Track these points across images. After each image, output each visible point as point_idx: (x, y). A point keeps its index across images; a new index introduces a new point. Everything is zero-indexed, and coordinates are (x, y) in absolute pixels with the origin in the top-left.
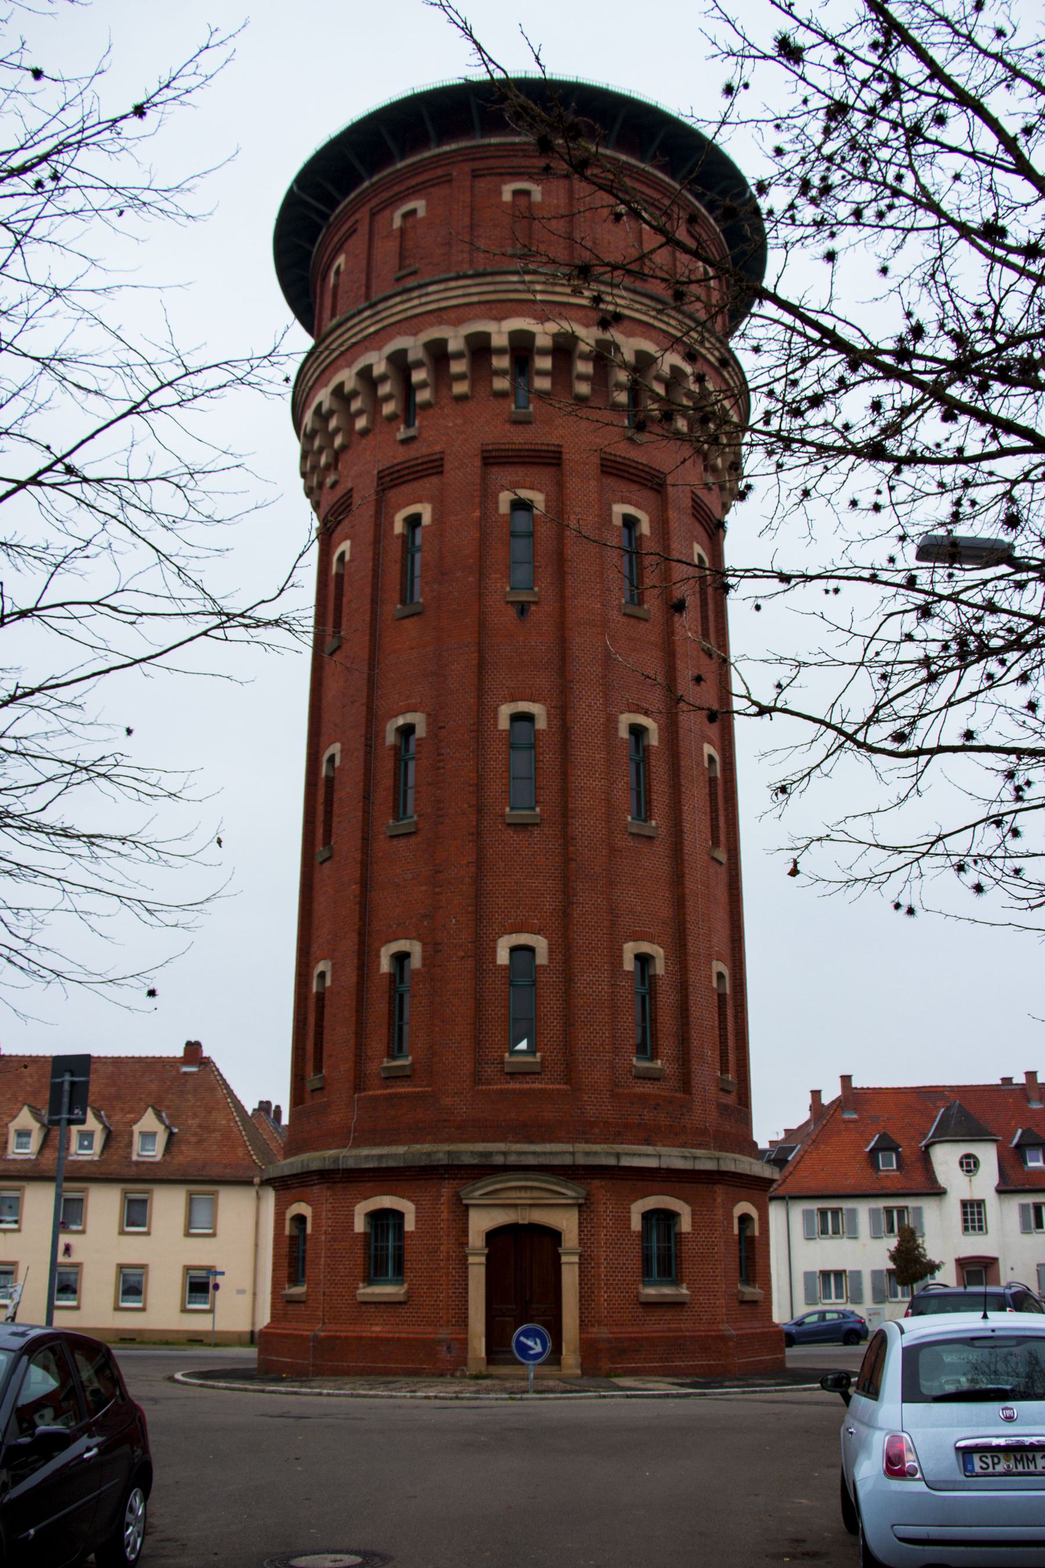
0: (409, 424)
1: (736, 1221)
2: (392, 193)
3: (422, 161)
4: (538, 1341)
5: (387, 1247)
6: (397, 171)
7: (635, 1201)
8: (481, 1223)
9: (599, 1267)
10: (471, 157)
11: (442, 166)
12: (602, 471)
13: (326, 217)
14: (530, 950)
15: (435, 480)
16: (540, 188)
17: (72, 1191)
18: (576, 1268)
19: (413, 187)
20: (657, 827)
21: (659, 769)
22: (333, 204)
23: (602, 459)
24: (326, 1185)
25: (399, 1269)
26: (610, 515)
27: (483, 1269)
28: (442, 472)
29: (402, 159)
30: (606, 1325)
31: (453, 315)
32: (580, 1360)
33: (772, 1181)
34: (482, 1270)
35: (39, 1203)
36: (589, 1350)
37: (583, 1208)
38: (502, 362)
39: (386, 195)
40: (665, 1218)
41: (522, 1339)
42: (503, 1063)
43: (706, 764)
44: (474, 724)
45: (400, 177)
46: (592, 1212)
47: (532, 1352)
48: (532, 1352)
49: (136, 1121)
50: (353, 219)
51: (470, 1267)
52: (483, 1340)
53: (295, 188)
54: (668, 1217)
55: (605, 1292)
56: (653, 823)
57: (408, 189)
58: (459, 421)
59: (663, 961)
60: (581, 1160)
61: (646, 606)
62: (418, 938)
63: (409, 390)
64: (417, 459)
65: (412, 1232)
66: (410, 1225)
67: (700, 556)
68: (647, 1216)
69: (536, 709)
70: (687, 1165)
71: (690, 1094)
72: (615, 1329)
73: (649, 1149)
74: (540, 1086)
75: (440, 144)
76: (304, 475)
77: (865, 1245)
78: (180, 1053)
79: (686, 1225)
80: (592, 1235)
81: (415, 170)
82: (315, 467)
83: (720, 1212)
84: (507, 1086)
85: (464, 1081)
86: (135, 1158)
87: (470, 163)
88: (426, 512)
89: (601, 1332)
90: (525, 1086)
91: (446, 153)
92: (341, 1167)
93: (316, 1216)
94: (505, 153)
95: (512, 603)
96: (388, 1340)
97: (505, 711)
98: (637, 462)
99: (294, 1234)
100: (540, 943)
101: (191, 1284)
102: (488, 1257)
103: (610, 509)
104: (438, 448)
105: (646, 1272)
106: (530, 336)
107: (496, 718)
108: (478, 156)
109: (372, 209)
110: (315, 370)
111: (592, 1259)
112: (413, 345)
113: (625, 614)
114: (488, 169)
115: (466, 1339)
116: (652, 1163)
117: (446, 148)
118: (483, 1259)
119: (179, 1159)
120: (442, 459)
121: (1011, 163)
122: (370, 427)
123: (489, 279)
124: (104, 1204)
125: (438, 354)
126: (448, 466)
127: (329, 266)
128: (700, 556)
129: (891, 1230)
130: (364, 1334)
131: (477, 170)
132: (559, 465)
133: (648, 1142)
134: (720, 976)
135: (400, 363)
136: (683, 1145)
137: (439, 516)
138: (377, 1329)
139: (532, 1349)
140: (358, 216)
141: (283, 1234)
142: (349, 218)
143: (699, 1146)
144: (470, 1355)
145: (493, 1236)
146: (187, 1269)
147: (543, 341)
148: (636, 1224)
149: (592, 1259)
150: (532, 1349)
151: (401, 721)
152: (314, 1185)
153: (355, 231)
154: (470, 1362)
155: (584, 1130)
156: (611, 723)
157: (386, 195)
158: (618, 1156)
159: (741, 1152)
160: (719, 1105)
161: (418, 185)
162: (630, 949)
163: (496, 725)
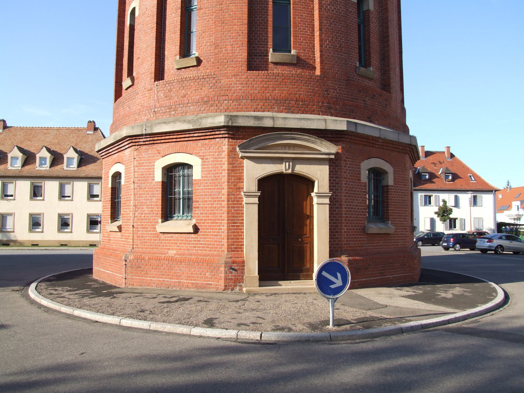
4: (339, 275)
7: (363, 160)
9: (341, 208)
17: (37, 182)
18: (327, 207)
27: (256, 208)
34: (255, 209)
35: (23, 187)
37: (334, 163)
40: (377, 174)
41: (324, 273)
46: (337, 166)
47: (333, 286)
48: (333, 286)
52: (257, 262)
55: (345, 226)
71: (390, 93)
78: (86, 126)
93: (127, 170)
101: (90, 221)
102: (260, 198)
118: (256, 200)
121: (226, 134)
124: (51, 188)
139: (334, 283)
141: (107, 187)
144: (246, 275)
145: (264, 182)
146: (89, 216)
150: (334, 283)
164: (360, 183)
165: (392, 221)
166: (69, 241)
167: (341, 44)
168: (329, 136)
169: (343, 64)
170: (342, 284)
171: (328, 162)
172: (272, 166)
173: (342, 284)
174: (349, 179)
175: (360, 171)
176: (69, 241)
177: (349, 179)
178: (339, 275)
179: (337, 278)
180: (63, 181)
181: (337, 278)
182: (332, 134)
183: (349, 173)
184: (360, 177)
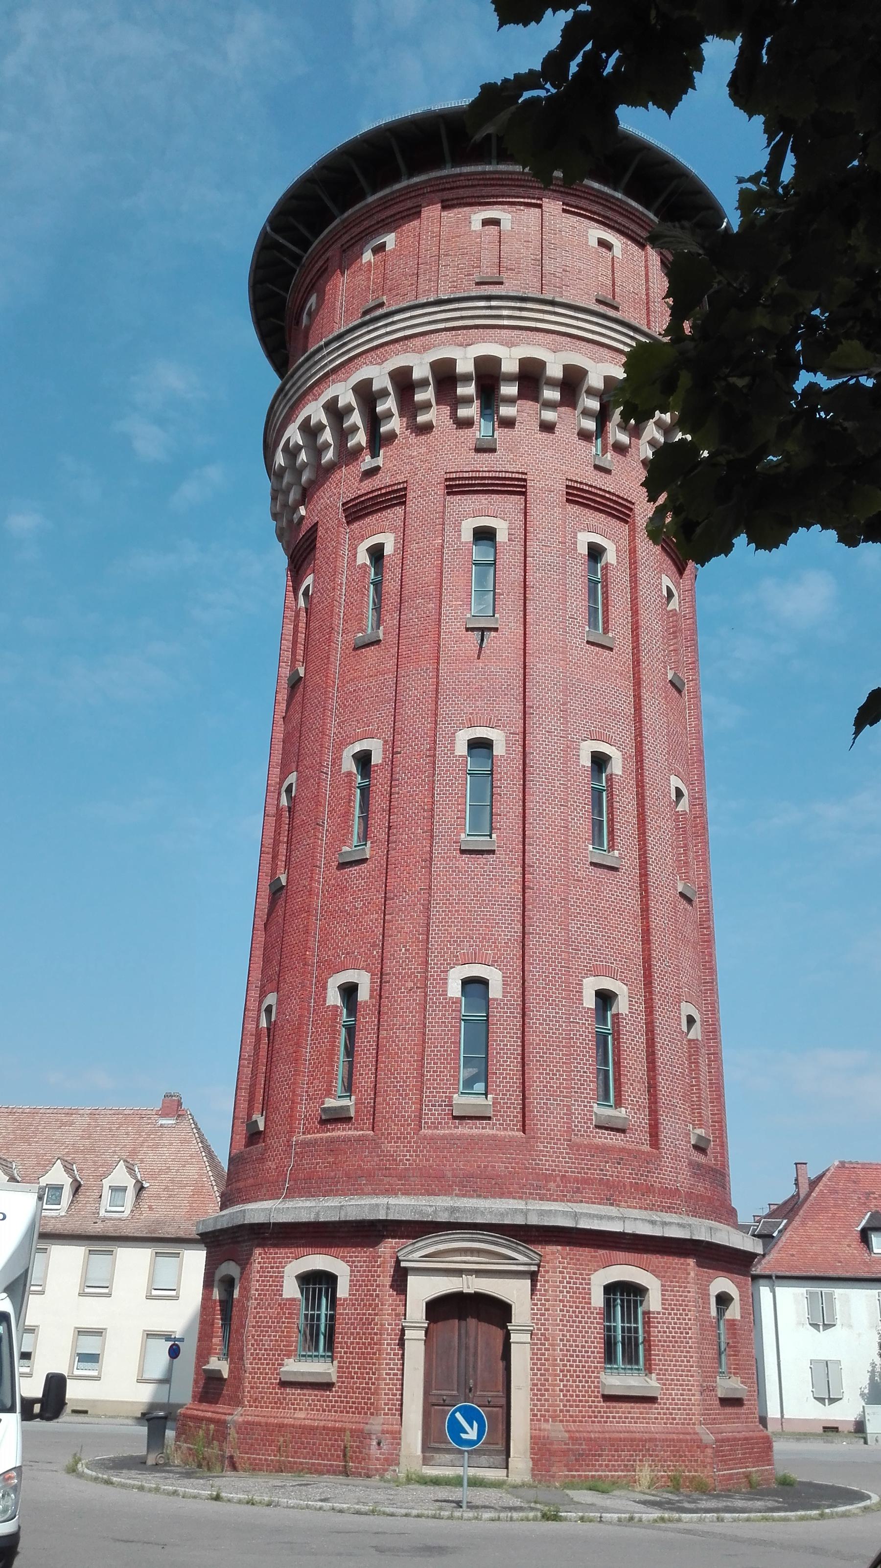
0: (374, 455)
1: (713, 1301)
2: (362, 228)
3: (393, 193)
4: (475, 1425)
5: (319, 1316)
6: (367, 205)
8: (423, 1290)
10: (441, 187)
11: (411, 198)
12: (568, 500)
13: (297, 259)
14: (483, 983)
15: (399, 510)
16: (509, 216)
19: (383, 220)
20: (620, 858)
21: (625, 801)
22: (305, 244)
23: (568, 487)
24: (256, 1242)
25: (330, 1345)
26: (575, 543)
28: (404, 503)
29: (374, 192)
30: (561, 1421)
31: (417, 342)
32: (530, 1464)
33: (754, 1255)
36: (542, 1451)
38: (468, 390)
39: (356, 230)
42: (451, 1106)
43: (674, 797)
44: (429, 750)
45: (369, 212)
47: (464, 1436)
48: (464, 1436)
49: (105, 1175)
50: (324, 257)
51: (406, 1342)
53: (268, 229)
54: (327, 1280)
56: (616, 853)
57: (378, 223)
58: (423, 450)
59: (627, 999)
60: (534, 1220)
61: (610, 635)
62: (367, 969)
63: (373, 421)
64: (380, 489)
65: (345, 1300)
66: (343, 1291)
67: (668, 588)
68: (610, 1289)
69: (495, 735)
70: (657, 1232)
72: (572, 1427)
73: (613, 1211)
74: (491, 1132)
75: (411, 175)
76: (275, 516)
77: (859, 1335)
79: (654, 1302)
80: (548, 1310)
81: (385, 204)
82: (285, 505)
83: (693, 1288)
84: (455, 1131)
85: (409, 1125)
86: (102, 1213)
87: (439, 194)
88: (389, 542)
89: (556, 1431)
90: (475, 1131)
91: (416, 184)
92: (272, 1221)
94: (476, 182)
95: (473, 629)
96: (313, 1429)
97: (463, 737)
98: (604, 491)
99: (223, 1299)
100: (494, 976)
103: (575, 537)
104: (401, 478)
105: (609, 1356)
106: (497, 361)
107: (453, 742)
108: (448, 186)
109: (342, 246)
110: (285, 407)
111: (547, 1339)
112: (379, 374)
113: (588, 642)
114: (457, 199)
115: (400, 1432)
116: (615, 1227)
117: (416, 180)
118: (422, 1334)
119: (146, 1214)
120: (405, 489)
122: (336, 460)
123: (456, 306)
125: (404, 383)
126: (410, 495)
127: (302, 309)
128: (668, 588)
129: (177, 1255)
130: (286, 1421)
131: (447, 200)
132: (524, 494)
133: (611, 1201)
134: (691, 1020)
135: (366, 394)
136: (652, 1208)
137: (403, 547)
138: (301, 1415)
139: (466, 1433)
140: (329, 254)
142: (320, 257)
143: (669, 1209)
144: (403, 1453)
147: (510, 366)
148: (598, 1299)
149: (547, 1339)
150: (466, 1433)
151: (357, 747)
152: (244, 1241)
153: (326, 269)
154: (402, 1460)
155: (539, 1185)
156: (571, 750)
157: (356, 230)
158: (576, 1216)
159: (718, 1219)
160: (691, 1164)
161: (387, 218)
162: (590, 986)
163: (452, 751)
164: (589, 1308)
165: (658, 1374)
166: (94, 1401)
167: (561, 1084)
168: (533, 1234)
169: (564, 1114)
170: (475, 1438)
171: (529, 1276)
172: (445, 1279)
173: (475, 1438)
174: (568, 1301)
175: (589, 1289)
176: (95, 1402)
177: (568, 1301)
178: (475, 1425)
179: (472, 1427)
180: (505, 1407)
181: (472, 1427)
182: (537, 1231)
183: (568, 1292)
184: (590, 1299)
